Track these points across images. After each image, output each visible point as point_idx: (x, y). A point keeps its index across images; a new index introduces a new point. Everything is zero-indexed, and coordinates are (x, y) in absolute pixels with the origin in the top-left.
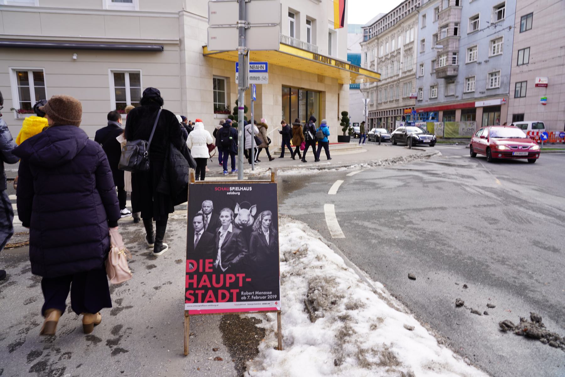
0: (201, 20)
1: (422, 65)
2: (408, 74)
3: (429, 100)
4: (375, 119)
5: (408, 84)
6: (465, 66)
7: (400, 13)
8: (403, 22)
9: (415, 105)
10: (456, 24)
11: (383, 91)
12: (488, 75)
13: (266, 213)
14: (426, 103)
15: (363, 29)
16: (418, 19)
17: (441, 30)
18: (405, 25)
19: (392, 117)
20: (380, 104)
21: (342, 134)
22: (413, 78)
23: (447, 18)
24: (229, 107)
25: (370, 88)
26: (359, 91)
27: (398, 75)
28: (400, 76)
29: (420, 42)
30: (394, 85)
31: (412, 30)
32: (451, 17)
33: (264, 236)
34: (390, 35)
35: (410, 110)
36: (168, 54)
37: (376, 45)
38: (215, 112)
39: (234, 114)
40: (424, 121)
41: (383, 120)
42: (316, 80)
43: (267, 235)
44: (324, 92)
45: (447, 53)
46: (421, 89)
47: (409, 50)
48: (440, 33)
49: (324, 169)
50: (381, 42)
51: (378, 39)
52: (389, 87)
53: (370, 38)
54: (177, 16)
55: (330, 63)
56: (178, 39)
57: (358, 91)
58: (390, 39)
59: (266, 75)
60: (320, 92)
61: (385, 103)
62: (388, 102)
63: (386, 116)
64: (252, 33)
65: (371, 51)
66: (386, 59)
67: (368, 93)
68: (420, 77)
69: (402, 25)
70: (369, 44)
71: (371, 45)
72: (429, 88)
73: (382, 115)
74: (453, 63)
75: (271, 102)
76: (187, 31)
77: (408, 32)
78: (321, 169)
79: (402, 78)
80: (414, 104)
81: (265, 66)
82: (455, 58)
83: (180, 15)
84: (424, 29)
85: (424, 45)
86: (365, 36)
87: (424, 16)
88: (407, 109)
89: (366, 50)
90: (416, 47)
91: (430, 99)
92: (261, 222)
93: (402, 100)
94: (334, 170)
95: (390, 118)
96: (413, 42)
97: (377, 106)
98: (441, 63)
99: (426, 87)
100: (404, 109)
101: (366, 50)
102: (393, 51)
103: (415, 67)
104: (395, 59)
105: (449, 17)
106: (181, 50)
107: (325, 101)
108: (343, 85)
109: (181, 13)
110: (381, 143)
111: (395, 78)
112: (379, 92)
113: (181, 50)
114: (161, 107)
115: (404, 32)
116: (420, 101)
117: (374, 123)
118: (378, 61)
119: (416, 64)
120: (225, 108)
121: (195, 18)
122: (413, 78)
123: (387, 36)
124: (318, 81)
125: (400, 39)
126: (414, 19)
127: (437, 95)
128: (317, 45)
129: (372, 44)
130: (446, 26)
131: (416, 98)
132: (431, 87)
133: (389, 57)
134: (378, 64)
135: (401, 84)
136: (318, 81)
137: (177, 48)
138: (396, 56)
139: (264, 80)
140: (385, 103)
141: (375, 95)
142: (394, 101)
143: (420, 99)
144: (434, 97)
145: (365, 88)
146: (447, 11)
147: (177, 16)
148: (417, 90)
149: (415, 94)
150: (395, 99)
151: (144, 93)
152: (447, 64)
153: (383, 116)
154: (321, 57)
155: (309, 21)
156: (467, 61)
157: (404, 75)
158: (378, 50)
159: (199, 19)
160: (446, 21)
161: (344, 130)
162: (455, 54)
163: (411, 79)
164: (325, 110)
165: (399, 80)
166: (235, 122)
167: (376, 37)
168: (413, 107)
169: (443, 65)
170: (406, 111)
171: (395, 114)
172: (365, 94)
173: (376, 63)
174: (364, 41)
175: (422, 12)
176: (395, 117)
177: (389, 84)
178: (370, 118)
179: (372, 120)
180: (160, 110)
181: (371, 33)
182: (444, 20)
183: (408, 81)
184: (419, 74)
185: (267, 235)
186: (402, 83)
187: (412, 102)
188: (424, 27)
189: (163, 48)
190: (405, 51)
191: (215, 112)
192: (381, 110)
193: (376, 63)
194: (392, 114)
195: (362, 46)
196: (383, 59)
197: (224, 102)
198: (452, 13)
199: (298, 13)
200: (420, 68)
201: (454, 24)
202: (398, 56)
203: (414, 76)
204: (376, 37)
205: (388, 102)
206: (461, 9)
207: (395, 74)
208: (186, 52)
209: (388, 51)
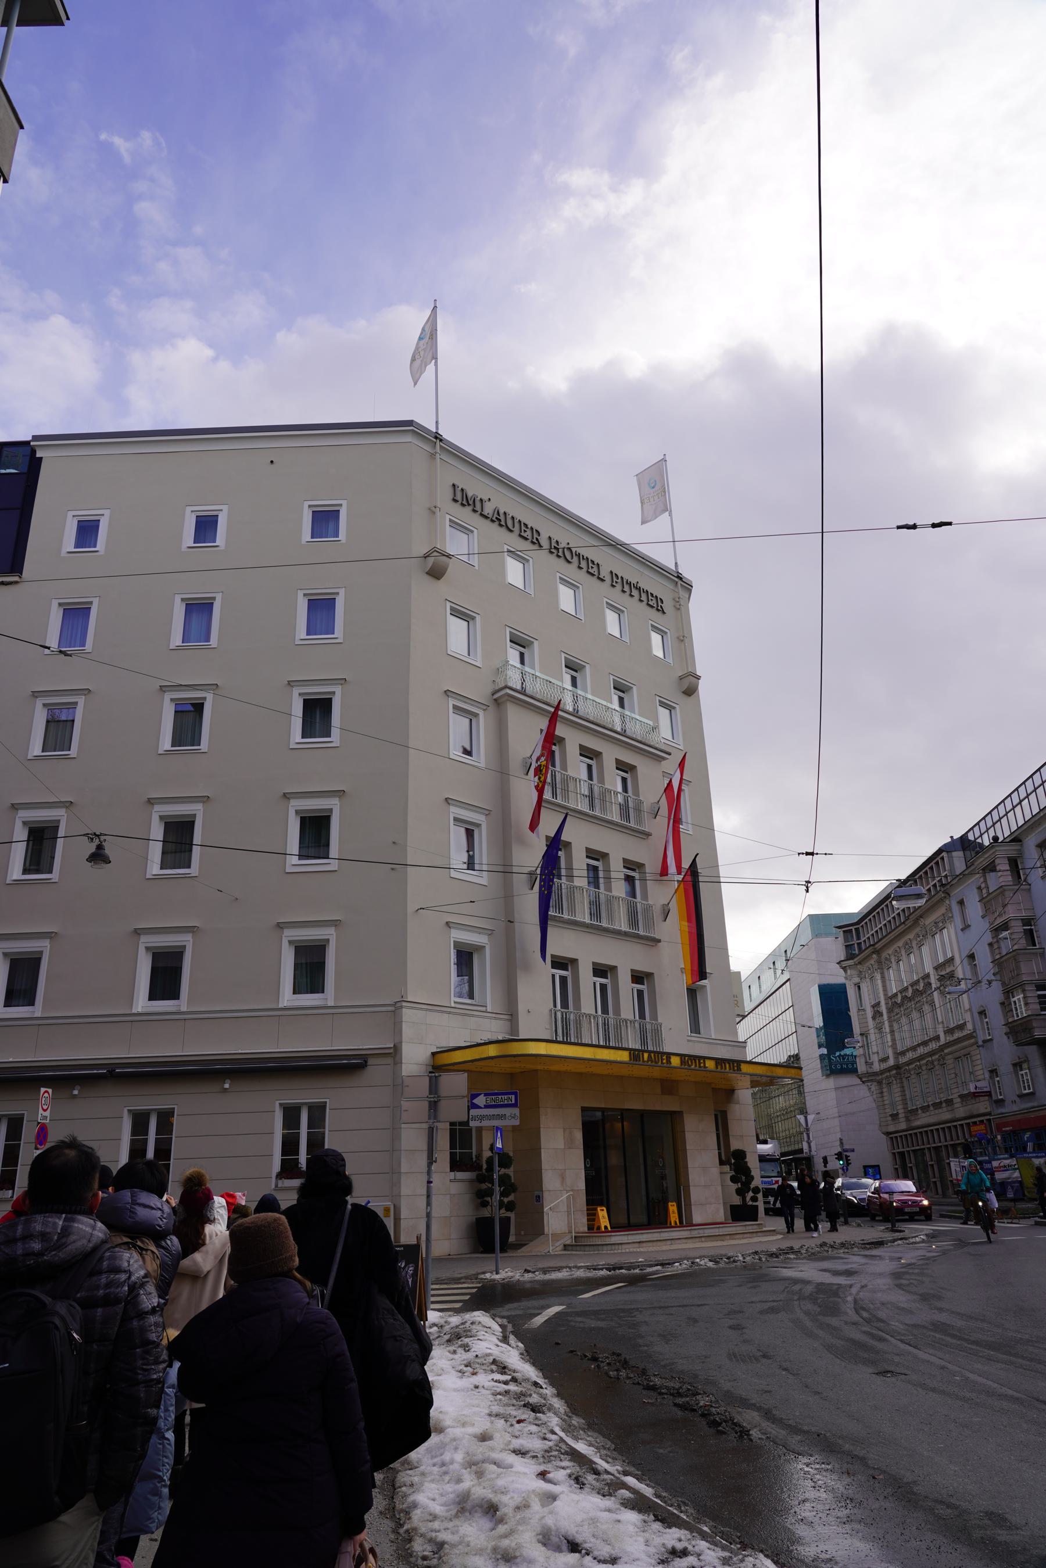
0: (430, 1010)
1: (982, 1013)
2: (958, 1035)
3: (1018, 1100)
5: (965, 1059)
7: (928, 884)
8: (921, 916)
9: (989, 1114)
10: (1027, 922)
13: (411, 1265)
14: (1015, 1108)
15: (841, 930)
17: (997, 936)
21: (737, 1200)
22: (972, 1045)
24: (479, 1156)
25: (882, 1072)
27: (937, 1038)
28: (943, 1040)
30: (936, 1063)
31: (945, 931)
32: (1009, 908)
33: (408, 1282)
35: (982, 1127)
36: (375, 1072)
37: (876, 966)
38: (452, 1170)
39: (487, 1170)
40: (1012, 1156)
43: (410, 1281)
44: (681, 1113)
45: (1022, 986)
46: (993, 1072)
47: (946, 974)
48: (998, 942)
49: (621, 1268)
50: (886, 959)
51: (878, 952)
52: (924, 1068)
53: (861, 951)
54: (392, 1008)
55: (669, 1061)
56: (392, 1046)
58: (903, 952)
59: (516, 1111)
60: (672, 1113)
61: (925, 1109)
64: (443, 1105)
66: (904, 998)
67: (880, 1083)
68: (984, 1041)
69: (922, 922)
70: (860, 963)
72: (1011, 1069)
75: (560, 1144)
76: (407, 1031)
77: (937, 936)
78: (614, 1269)
79: (948, 1045)
80: (988, 1110)
81: (513, 1096)
83: (395, 1010)
84: (967, 931)
85: (975, 965)
86: (848, 947)
87: (961, 903)
88: (975, 1123)
89: (857, 980)
91: (1021, 1096)
92: (407, 1272)
93: (959, 1100)
94: (637, 1271)
96: (952, 959)
97: (908, 1119)
98: (1016, 1010)
99: (1005, 1067)
100: (968, 1124)
101: (857, 980)
103: (968, 1017)
106: (395, 1064)
109: (398, 1005)
110: (850, 1219)
111: (933, 1046)
113: (395, 1064)
114: (348, 1198)
115: (929, 937)
116: (1000, 1102)
118: (887, 1004)
119: (970, 1010)
120: (472, 1158)
121: (421, 1009)
122: (972, 1045)
125: (925, 950)
126: (942, 910)
127: (1033, 1087)
128: (660, 1020)
130: (1005, 926)
131: (989, 1094)
132: (1015, 1065)
133: (910, 993)
134: (890, 1011)
135: (949, 1060)
137: (389, 1060)
139: (513, 1120)
140: (925, 1109)
141: (896, 1089)
143: (1000, 1097)
144: (1027, 1091)
145: (870, 1071)
146: (998, 895)
147: (392, 1008)
148: (987, 1075)
149: (984, 1085)
152: (1029, 1013)
154: (646, 1055)
155: (638, 977)
157: (950, 1038)
158: (883, 977)
159: (427, 1010)
161: (740, 1192)
163: (966, 1047)
164: (685, 1150)
165: (942, 1048)
166: (490, 1185)
167: (871, 949)
168: (988, 1117)
169: (1022, 1014)
170: (974, 1129)
172: (874, 1087)
173: (883, 1008)
174: (850, 956)
175: (956, 893)
177: (924, 1062)
179: (902, 1154)
180: (349, 1207)
181: (863, 939)
183: (963, 1052)
184: (982, 1036)
185: (410, 1281)
186: (950, 1057)
187: (983, 1106)
188: (966, 927)
189: (366, 1062)
190: (939, 980)
191: (452, 1170)
192: (918, 1128)
193: (883, 1008)
195: (844, 969)
196: (899, 999)
197: (472, 1149)
199: (613, 969)
200: (981, 1019)
201: (1020, 923)
203: (972, 1041)
204: (871, 949)
206: (1029, 890)
208: (404, 1066)
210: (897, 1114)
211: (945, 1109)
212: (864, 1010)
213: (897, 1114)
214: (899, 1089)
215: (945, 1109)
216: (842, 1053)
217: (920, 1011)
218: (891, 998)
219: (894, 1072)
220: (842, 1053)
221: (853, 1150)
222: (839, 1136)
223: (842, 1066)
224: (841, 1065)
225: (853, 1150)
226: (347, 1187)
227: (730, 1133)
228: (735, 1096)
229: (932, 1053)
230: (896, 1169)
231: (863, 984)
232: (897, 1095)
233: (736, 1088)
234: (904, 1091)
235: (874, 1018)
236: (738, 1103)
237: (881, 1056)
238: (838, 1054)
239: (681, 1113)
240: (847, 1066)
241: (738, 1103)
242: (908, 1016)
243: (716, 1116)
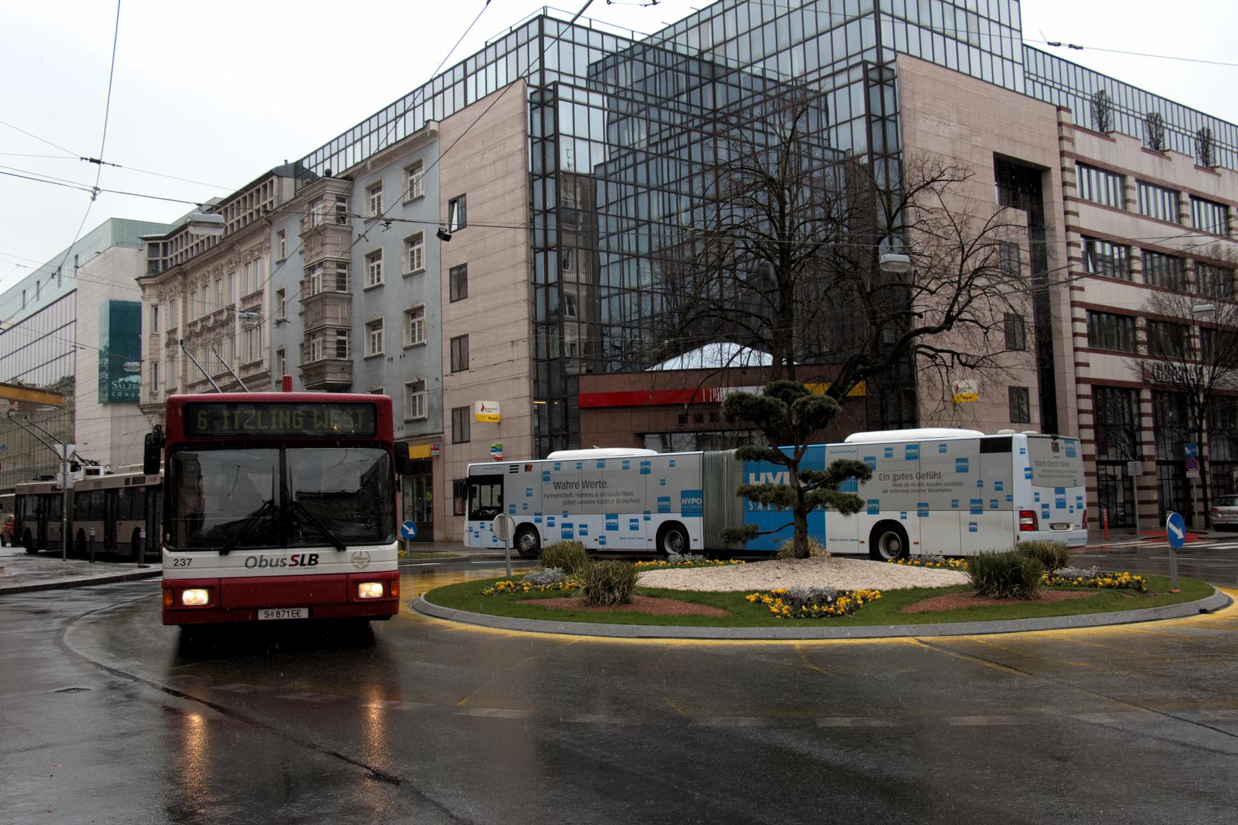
2: (253, 372)
6: (364, 363)
12: (364, 258)
16: (269, 239)
18: (245, 248)
23: (319, 249)
26: (137, 411)
29: (275, 295)
34: (210, 268)
37: (179, 289)
50: (192, 283)
51: (185, 274)
57: (134, 411)
65: (168, 302)
70: (162, 283)
71: (167, 288)
74: (339, 355)
82: (344, 342)
89: (155, 301)
90: (268, 304)
101: (155, 301)
102: (208, 314)
103: (266, 356)
105: (324, 248)
115: (242, 265)
118: (184, 331)
119: (269, 348)
123: (204, 270)
129: (171, 286)
145: (154, 402)
156: (367, 353)
160: (317, 254)
162: (341, 265)
182: (314, 253)
195: (143, 287)
198: (328, 240)
209: (209, 310)
212: (158, 336)
216: (127, 379)
218: (190, 326)
235: (168, 345)
237: (169, 387)
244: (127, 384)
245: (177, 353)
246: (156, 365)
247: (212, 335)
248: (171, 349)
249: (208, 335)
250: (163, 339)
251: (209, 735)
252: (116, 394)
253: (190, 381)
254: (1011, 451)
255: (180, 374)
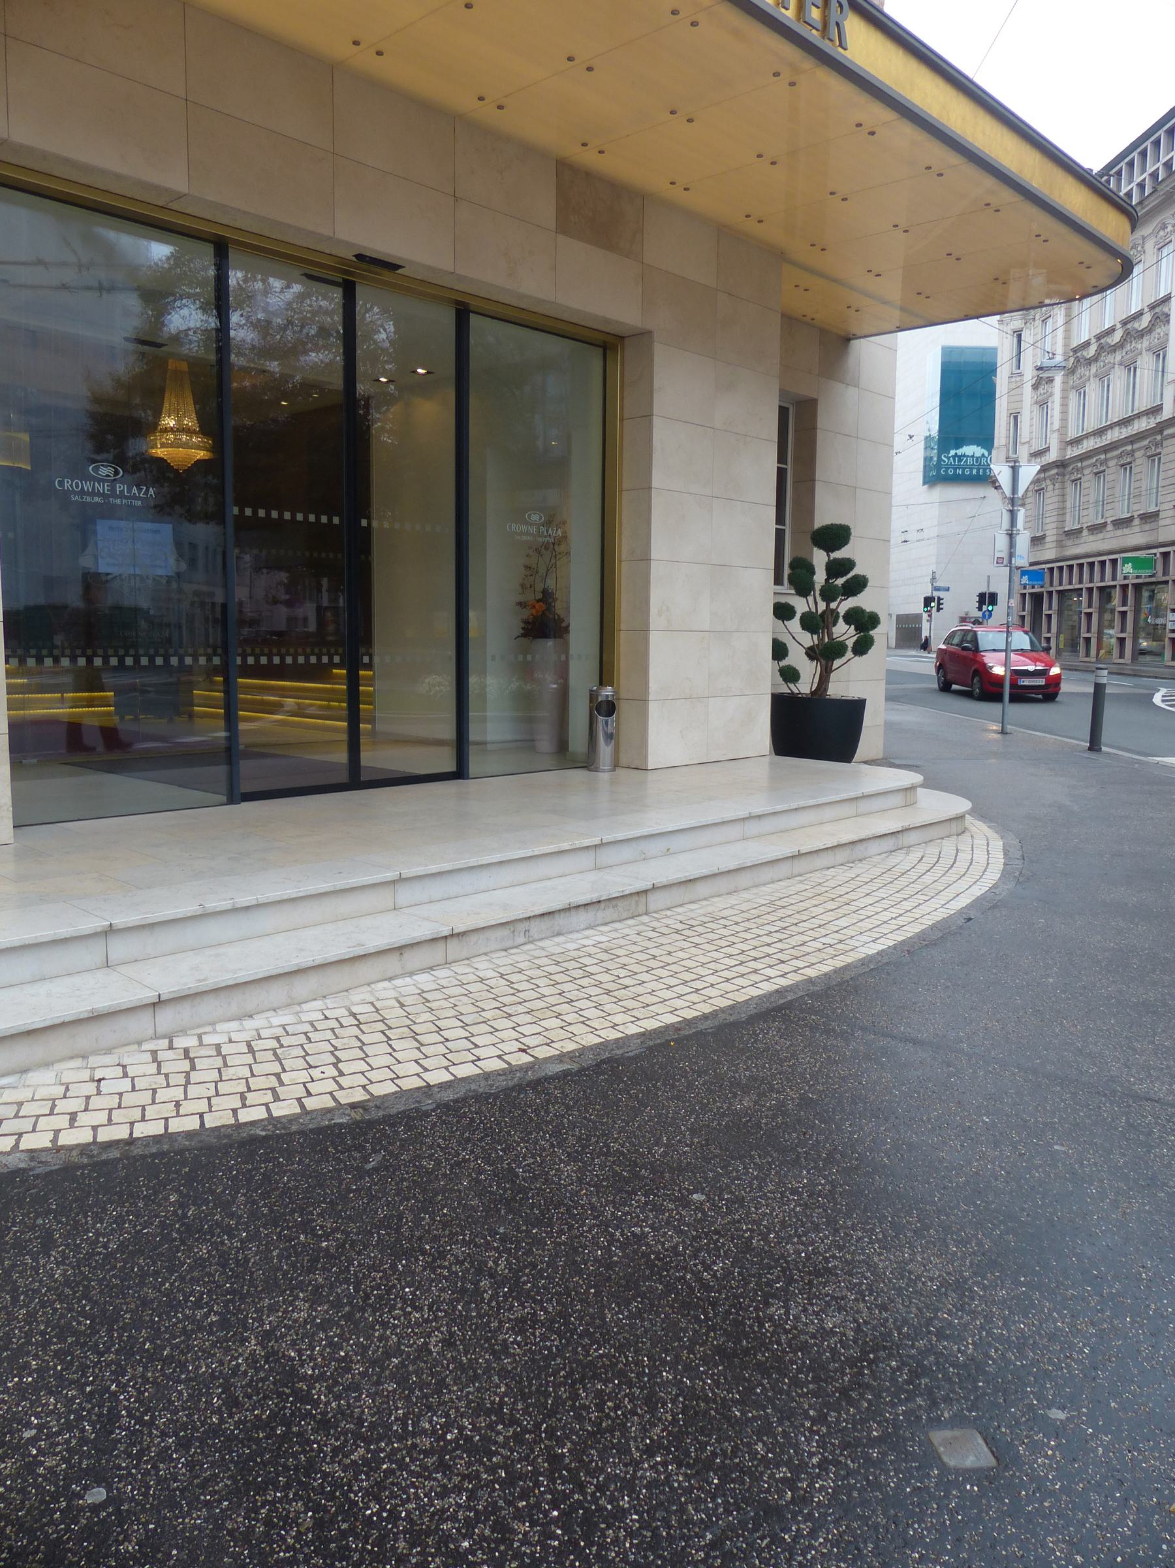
4: (1050, 593)
11: (1088, 479)
19: (1090, 590)
20: (1075, 533)
27: (1158, 409)
41: (1117, 595)
42: (545, 207)
44: (644, 336)
61: (1095, 529)
62: (1110, 527)
63: (1097, 583)
73: (1081, 582)
95: (1117, 595)
97: (1060, 545)
104: (1145, 343)
107: (649, 416)
108: (846, 340)
111: (1143, 424)
112: (1068, 484)
117: (1046, 612)
124: (563, 227)
136: (563, 227)
138: (1149, 330)
140: (1095, 529)
142: (1137, 521)
150: (1139, 509)
151: (821, 590)
153: (1086, 585)
165: (1160, 428)
171: (1102, 579)
176: (1101, 589)
178: (1028, 591)
179: (1037, 599)
194: (1091, 580)
202: (1160, 330)
205: (1110, 527)
207: (1143, 403)
210: (1043, 538)
211: (1137, 529)
212: (1021, 375)
213: (1043, 538)
214: (1056, 499)
215: (1137, 529)
216: (959, 452)
217: (1131, 367)
218: (1075, 351)
219: (1054, 471)
220: (959, 452)
221: (948, 589)
222: (933, 568)
223: (955, 471)
224: (955, 469)
225: (948, 589)
226: (874, 627)
227: (819, 475)
228: (851, 360)
229: (1132, 439)
230: (1023, 617)
231: (1028, 332)
232: (1050, 507)
233: (854, 329)
234: (1064, 501)
235: (1035, 387)
236: (857, 386)
237: (1036, 447)
238: (952, 452)
239: (644, 336)
240: (963, 472)
241: (857, 386)
242: (1102, 377)
243: (783, 412)
244: (960, 457)
245: (1051, 395)
246: (1016, 418)
247: (1118, 356)
248: (1041, 390)
249: (1110, 358)
250: (1029, 373)
251: (150, 267)
252: (946, 471)
253: (1072, 434)
254: (773, 695)
255: (1056, 426)
